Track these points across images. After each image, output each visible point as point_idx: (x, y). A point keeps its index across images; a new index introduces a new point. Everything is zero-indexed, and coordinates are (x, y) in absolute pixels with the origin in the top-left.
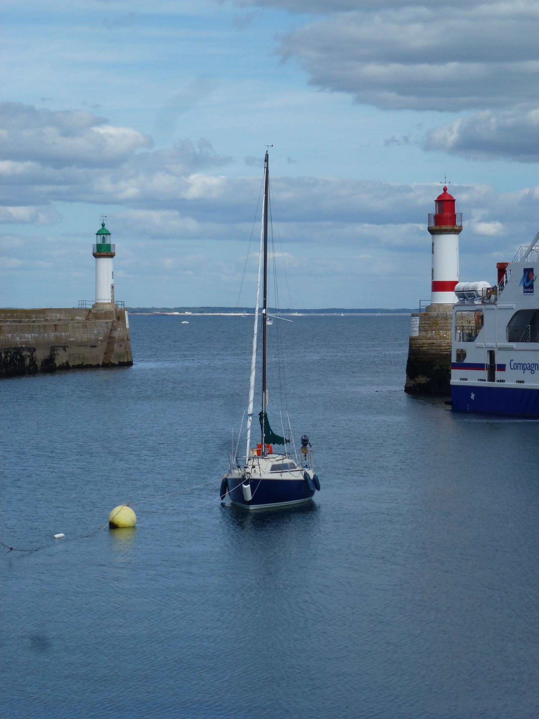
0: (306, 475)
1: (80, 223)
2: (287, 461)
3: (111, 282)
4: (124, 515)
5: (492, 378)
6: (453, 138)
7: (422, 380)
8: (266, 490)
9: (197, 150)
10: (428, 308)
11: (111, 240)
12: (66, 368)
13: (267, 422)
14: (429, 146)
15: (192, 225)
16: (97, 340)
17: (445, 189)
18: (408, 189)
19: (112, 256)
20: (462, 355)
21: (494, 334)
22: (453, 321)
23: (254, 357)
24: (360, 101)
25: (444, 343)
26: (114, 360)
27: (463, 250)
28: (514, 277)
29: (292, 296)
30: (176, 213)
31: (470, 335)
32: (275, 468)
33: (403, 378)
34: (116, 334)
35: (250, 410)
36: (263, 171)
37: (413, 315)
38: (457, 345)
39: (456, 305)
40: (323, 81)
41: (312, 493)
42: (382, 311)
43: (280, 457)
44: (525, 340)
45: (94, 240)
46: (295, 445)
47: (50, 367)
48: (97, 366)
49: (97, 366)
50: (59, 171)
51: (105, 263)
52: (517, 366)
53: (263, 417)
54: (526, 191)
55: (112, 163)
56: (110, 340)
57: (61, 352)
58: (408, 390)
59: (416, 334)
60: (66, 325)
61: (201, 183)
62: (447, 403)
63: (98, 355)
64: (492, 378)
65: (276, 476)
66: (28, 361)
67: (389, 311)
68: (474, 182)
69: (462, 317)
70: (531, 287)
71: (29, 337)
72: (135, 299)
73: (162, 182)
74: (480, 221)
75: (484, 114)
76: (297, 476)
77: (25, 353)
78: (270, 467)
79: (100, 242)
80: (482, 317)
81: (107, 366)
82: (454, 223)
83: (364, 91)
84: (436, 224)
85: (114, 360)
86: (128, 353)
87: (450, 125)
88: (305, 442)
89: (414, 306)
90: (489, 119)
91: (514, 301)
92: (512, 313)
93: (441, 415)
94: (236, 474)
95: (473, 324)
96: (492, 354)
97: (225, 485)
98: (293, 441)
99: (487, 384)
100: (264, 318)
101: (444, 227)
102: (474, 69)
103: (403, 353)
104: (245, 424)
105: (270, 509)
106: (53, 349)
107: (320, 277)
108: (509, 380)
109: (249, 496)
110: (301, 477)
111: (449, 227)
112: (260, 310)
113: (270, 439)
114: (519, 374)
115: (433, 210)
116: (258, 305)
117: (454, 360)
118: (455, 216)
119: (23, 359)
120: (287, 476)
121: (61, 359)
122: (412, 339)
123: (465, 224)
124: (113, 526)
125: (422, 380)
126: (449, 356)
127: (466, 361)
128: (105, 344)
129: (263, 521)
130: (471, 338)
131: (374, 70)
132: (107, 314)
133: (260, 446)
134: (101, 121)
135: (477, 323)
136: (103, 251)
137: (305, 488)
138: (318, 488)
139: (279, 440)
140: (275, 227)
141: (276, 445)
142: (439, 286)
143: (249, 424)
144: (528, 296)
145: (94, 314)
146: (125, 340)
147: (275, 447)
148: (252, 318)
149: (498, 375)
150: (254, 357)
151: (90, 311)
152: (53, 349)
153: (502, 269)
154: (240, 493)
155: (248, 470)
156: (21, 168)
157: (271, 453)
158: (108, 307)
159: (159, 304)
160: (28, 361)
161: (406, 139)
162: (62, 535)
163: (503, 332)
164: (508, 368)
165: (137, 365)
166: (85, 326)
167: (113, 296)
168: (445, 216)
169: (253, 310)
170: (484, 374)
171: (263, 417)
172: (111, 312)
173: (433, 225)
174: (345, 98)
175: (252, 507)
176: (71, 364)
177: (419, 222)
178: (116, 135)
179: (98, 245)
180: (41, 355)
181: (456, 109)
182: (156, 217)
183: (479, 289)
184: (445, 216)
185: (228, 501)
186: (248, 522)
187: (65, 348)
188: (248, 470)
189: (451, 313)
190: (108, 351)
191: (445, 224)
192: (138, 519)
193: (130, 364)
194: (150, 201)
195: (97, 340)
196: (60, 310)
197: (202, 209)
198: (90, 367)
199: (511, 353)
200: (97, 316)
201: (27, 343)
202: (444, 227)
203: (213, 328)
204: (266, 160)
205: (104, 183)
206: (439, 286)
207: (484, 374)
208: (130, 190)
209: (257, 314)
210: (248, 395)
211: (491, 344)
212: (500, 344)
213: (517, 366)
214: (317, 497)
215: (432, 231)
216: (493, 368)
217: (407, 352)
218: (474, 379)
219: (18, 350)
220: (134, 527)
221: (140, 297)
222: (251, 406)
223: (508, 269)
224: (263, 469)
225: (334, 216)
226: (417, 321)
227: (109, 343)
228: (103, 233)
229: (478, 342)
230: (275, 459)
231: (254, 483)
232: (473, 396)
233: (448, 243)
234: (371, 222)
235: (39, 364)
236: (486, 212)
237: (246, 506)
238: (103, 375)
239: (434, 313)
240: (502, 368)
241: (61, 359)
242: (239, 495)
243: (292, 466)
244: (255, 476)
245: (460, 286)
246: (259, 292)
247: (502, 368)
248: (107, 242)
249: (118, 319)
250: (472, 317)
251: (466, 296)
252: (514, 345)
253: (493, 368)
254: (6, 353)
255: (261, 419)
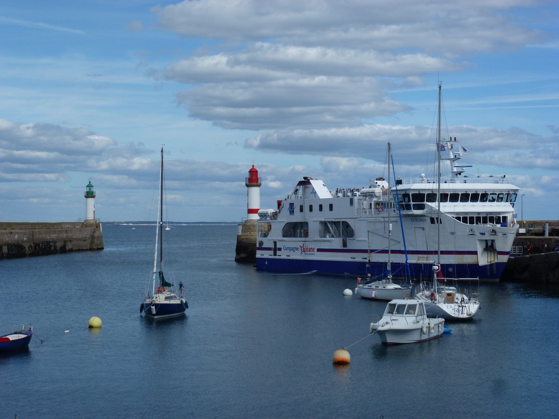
0: (182, 301)
1: (78, 181)
2: (172, 295)
3: (93, 209)
4: (96, 321)
5: (275, 254)
6: (256, 142)
7: (243, 255)
8: (162, 309)
9: (137, 147)
10: (246, 222)
11: (93, 190)
12: (71, 251)
13: (163, 276)
14: (247, 146)
15: (133, 182)
16: (86, 237)
17: (253, 166)
18: (238, 166)
19: (94, 197)
20: (261, 243)
21: (276, 234)
22: (257, 228)
23: (157, 245)
24: (215, 124)
25: (253, 238)
26: (94, 246)
27: (262, 194)
28: (286, 206)
29: (175, 216)
30: (126, 177)
31: (265, 234)
32: (167, 298)
33: (234, 255)
34: (96, 234)
35: (155, 270)
36: (160, 156)
37: (239, 225)
38: (259, 239)
39: (258, 220)
40: (195, 115)
41: (184, 310)
42: (224, 223)
43: (169, 293)
44: (290, 236)
45: (85, 190)
46: (177, 286)
47: (63, 250)
48: (87, 250)
49: (87, 250)
50: (71, 156)
51: (91, 201)
52: (287, 249)
53: (161, 274)
54: (292, 167)
55: (98, 153)
56: (93, 237)
57: (69, 243)
58: (236, 260)
59: (240, 234)
60: (72, 230)
61: (139, 163)
62: (254, 266)
63: (87, 245)
64: (275, 254)
65: (167, 302)
66: (53, 248)
67: (227, 223)
68: (265, 162)
69: (262, 226)
70: (293, 212)
71: (54, 236)
72: (105, 217)
73: (120, 162)
74: (270, 181)
75: (272, 131)
76: (177, 302)
77: (51, 244)
78: (164, 297)
79: (88, 190)
80: (271, 226)
81: (91, 249)
82: (257, 182)
83: (215, 119)
84: (249, 182)
85: (94, 246)
86: (101, 243)
87: (256, 137)
88: (181, 286)
89: (239, 220)
90: (274, 135)
91: (285, 218)
92: (284, 224)
93: (251, 271)
94: (148, 301)
95: (267, 229)
96: (275, 243)
97: (142, 307)
98: (175, 285)
99: (273, 257)
100: (161, 227)
101: (253, 184)
102: (267, 111)
103: (234, 243)
104: (152, 277)
105: (164, 318)
106: (65, 242)
107: (187, 207)
108: (283, 255)
109: (154, 312)
110: (179, 302)
111: (255, 184)
112: (159, 222)
113: (164, 284)
114: (288, 252)
115: (248, 176)
116: (158, 220)
117: (258, 246)
118: (258, 178)
119: (50, 246)
120: (172, 302)
121: (69, 246)
122: (238, 236)
123: (263, 183)
124: (91, 327)
125: (243, 255)
126: (255, 244)
127: (263, 246)
128: (90, 239)
129: (161, 323)
130: (265, 235)
131: (221, 110)
132: (91, 225)
133: (159, 288)
134: (92, 133)
135: (268, 228)
136: (90, 195)
137: (182, 307)
138: (187, 307)
139: (169, 285)
140: (166, 183)
141: (167, 287)
142: (251, 211)
143: (154, 277)
144: (292, 216)
145: (85, 225)
146: (100, 238)
147: (167, 288)
148: (156, 226)
149: (278, 253)
150: (157, 245)
151: (83, 223)
152: (65, 242)
153: (279, 203)
154: (150, 311)
155: (154, 299)
156: (52, 155)
157: (164, 291)
158: (92, 222)
159: (117, 220)
160: (53, 248)
161: (236, 143)
162: (66, 331)
163: (280, 233)
164: (282, 249)
165: (106, 249)
166: (80, 231)
167: (94, 216)
168: (253, 179)
169: (156, 222)
170: (272, 252)
171: (161, 274)
172: (93, 224)
173: (248, 183)
174: (210, 123)
175: (156, 317)
176: (74, 249)
177: (242, 181)
178: (99, 140)
179: (87, 192)
180: (59, 245)
181: (257, 129)
182: (115, 179)
183: (269, 212)
184: (253, 179)
185: (143, 314)
186: (154, 324)
187: (71, 241)
188: (154, 299)
189: (256, 224)
190: (92, 242)
191: (253, 182)
192: (103, 322)
193: (102, 249)
194: (113, 171)
195: (86, 237)
196: (68, 223)
197: (138, 175)
198: (83, 250)
199: (284, 242)
200: (86, 226)
201: (52, 239)
202: (253, 184)
203: (141, 231)
204: (162, 152)
205: (92, 162)
206: (251, 211)
207: (272, 252)
208: (104, 165)
209: (158, 224)
210: (153, 264)
211: (275, 238)
212: (279, 238)
213: (287, 249)
214: (187, 312)
215: (247, 186)
216: (276, 250)
217: (236, 242)
218: (267, 255)
219: (48, 243)
220: (100, 327)
221: (108, 216)
222: (155, 268)
223: (282, 204)
224: (161, 299)
225: (198, 178)
226: (240, 227)
227: (92, 239)
228: (90, 186)
229: (269, 237)
230: (167, 294)
231: (157, 305)
232: (266, 263)
233: (255, 191)
234: (220, 181)
235: (58, 249)
236: (273, 177)
237: (153, 317)
238: (90, 253)
239: (248, 224)
240: (280, 249)
241: (69, 246)
242: (149, 311)
243: (175, 297)
244: (158, 302)
245: (260, 211)
246: (159, 214)
247: (280, 249)
248: (92, 190)
249: (97, 227)
250: (266, 225)
251: (263, 216)
252: (285, 239)
253: (276, 250)
254: (42, 244)
255: (160, 275)
